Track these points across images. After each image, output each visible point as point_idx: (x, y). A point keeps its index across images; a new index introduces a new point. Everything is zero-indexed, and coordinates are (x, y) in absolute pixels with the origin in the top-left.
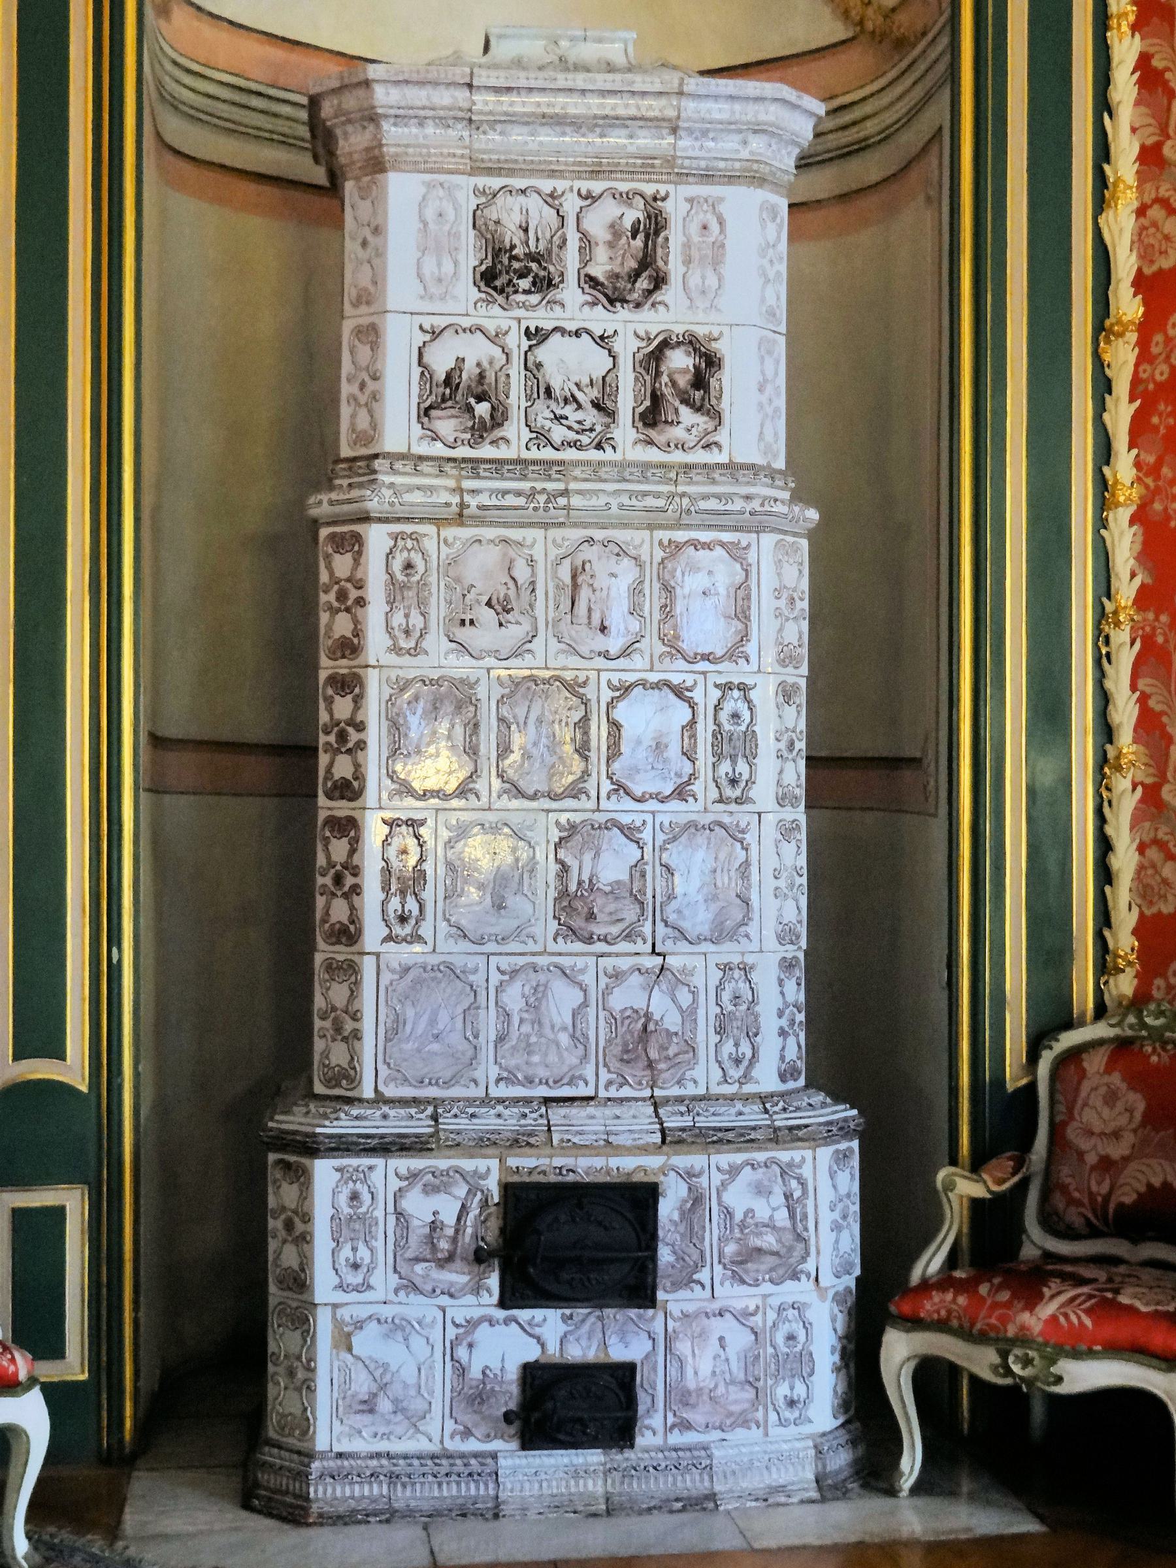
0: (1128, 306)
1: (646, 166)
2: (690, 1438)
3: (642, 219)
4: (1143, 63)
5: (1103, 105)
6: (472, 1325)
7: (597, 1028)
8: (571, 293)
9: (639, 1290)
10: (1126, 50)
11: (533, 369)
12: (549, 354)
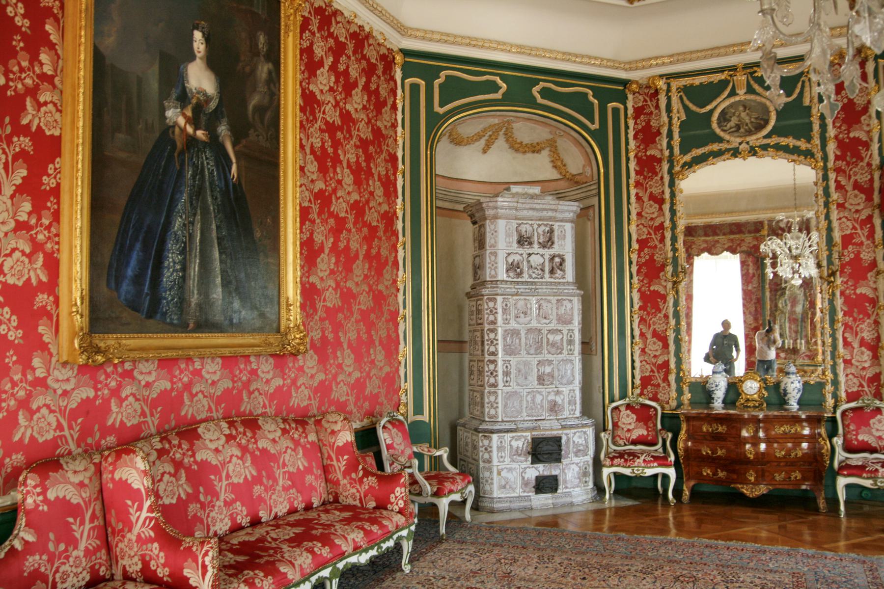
0: (635, 246)
1: (550, 219)
2: (567, 490)
3: (738, 330)
4: (637, 194)
5: (629, 203)
6: (525, 468)
7: (546, 405)
8: (536, 246)
9: (558, 460)
10: (633, 192)
11: (529, 262)
12: (532, 258)
